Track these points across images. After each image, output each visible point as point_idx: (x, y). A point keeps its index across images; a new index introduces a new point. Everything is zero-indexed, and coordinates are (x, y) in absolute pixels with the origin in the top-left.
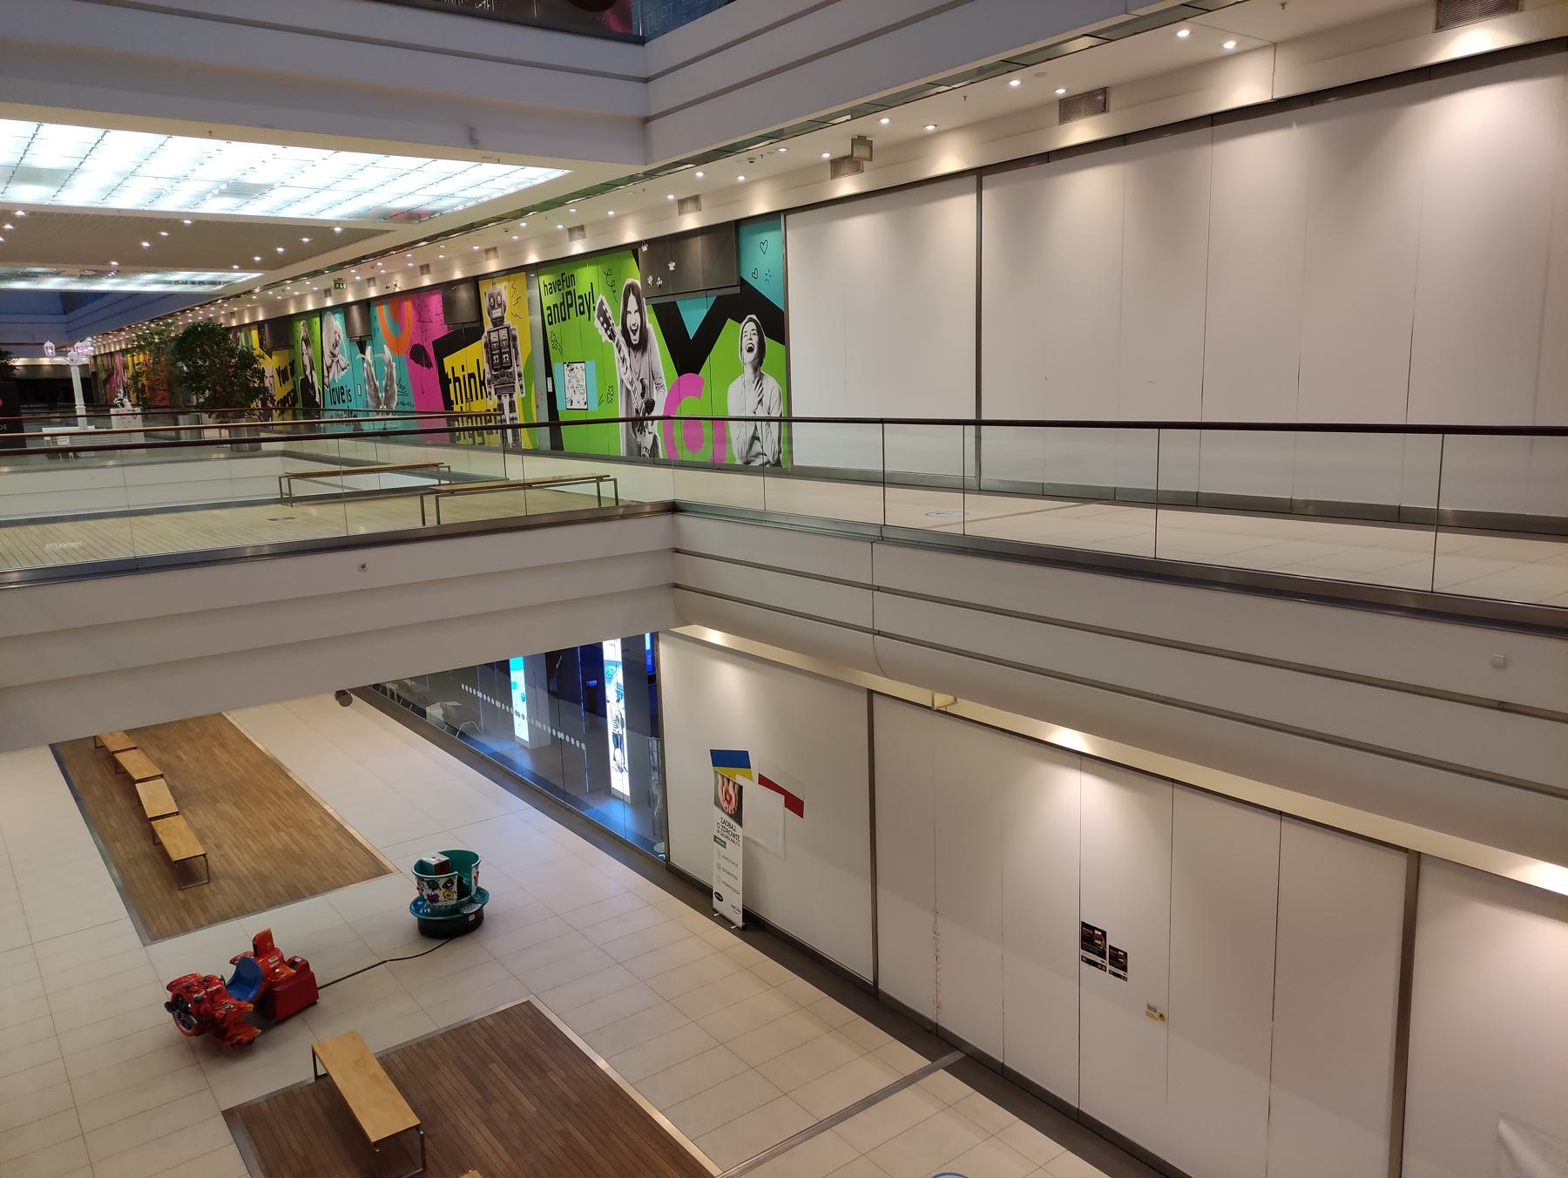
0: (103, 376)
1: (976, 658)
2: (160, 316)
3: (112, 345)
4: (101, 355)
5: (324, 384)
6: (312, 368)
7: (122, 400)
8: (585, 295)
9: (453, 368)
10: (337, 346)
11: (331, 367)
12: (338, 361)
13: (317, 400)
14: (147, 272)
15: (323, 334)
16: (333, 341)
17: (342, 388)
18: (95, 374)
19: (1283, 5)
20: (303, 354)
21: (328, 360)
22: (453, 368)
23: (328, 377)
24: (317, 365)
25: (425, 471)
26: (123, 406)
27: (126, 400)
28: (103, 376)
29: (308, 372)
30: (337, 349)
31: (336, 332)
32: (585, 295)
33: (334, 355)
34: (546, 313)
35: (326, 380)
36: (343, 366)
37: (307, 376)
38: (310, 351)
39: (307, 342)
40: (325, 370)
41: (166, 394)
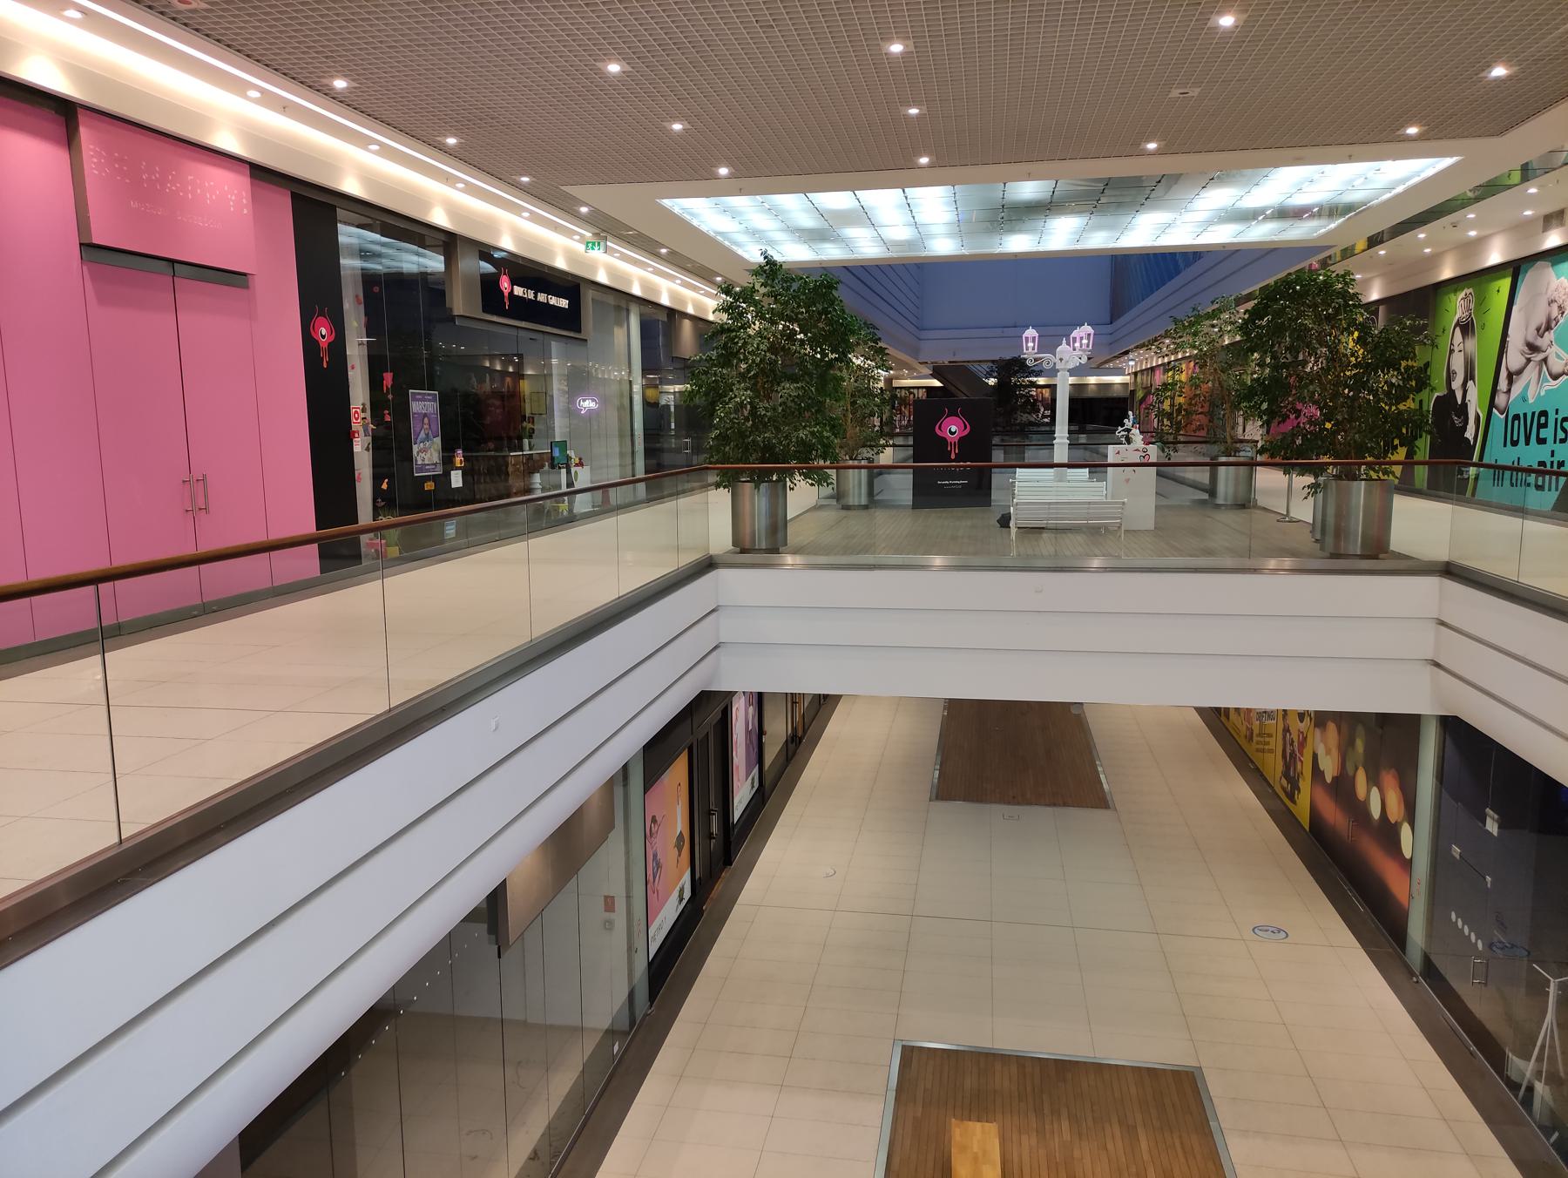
0: (1140, 394)
1: (1237, 741)
2: (1115, 355)
3: (1155, 359)
4: (1142, 371)
5: (1492, 404)
6: (1469, 375)
7: (1128, 430)
8: (1525, 415)
9: (1519, 459)
10: (1548, 328)
11: (1520, 372)
12: (1545, 360)
13: (1469, 434)
14: (1211, 181)
15: (1515, 308)
16: (1540, 319)
17: (1544, 413)
18: (1133, 392)
19: (741, 189)
20: (1452, 351)
21: (1514, 359)
22: (1519, 459)
23: (1509, 391)
24: (1484, 372)
25: (1403, 565)
26: (1129, 441)
27: (1135, 431)
28: (1140, 394)
29: (1456, 385)
30: (1549, 336)
31: (1551, 302)
32: (1525, 415)
33: (1533, 348)
34: (1278, 460)
35: (1501, 400)
36: (1557, 369)
37: (1452, 393)
38: (1471, 344)
39: (1467, 328)
40: (1502, 376)
41: (1203, 420)
